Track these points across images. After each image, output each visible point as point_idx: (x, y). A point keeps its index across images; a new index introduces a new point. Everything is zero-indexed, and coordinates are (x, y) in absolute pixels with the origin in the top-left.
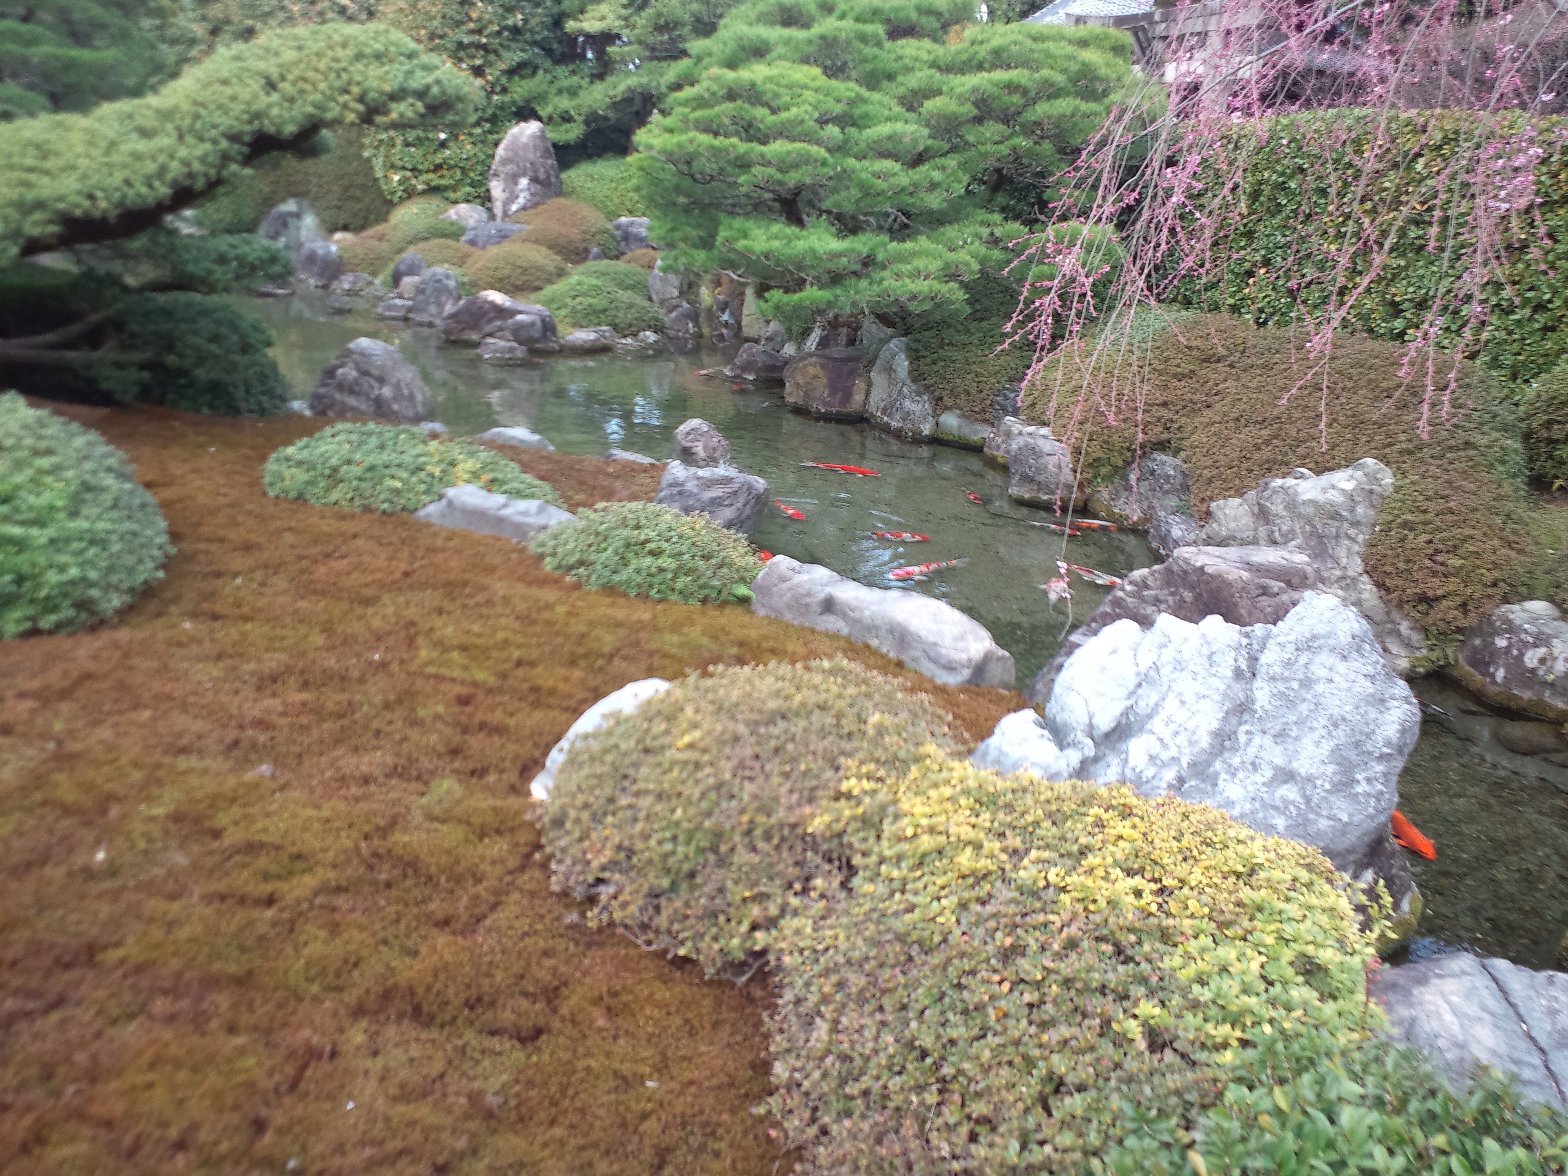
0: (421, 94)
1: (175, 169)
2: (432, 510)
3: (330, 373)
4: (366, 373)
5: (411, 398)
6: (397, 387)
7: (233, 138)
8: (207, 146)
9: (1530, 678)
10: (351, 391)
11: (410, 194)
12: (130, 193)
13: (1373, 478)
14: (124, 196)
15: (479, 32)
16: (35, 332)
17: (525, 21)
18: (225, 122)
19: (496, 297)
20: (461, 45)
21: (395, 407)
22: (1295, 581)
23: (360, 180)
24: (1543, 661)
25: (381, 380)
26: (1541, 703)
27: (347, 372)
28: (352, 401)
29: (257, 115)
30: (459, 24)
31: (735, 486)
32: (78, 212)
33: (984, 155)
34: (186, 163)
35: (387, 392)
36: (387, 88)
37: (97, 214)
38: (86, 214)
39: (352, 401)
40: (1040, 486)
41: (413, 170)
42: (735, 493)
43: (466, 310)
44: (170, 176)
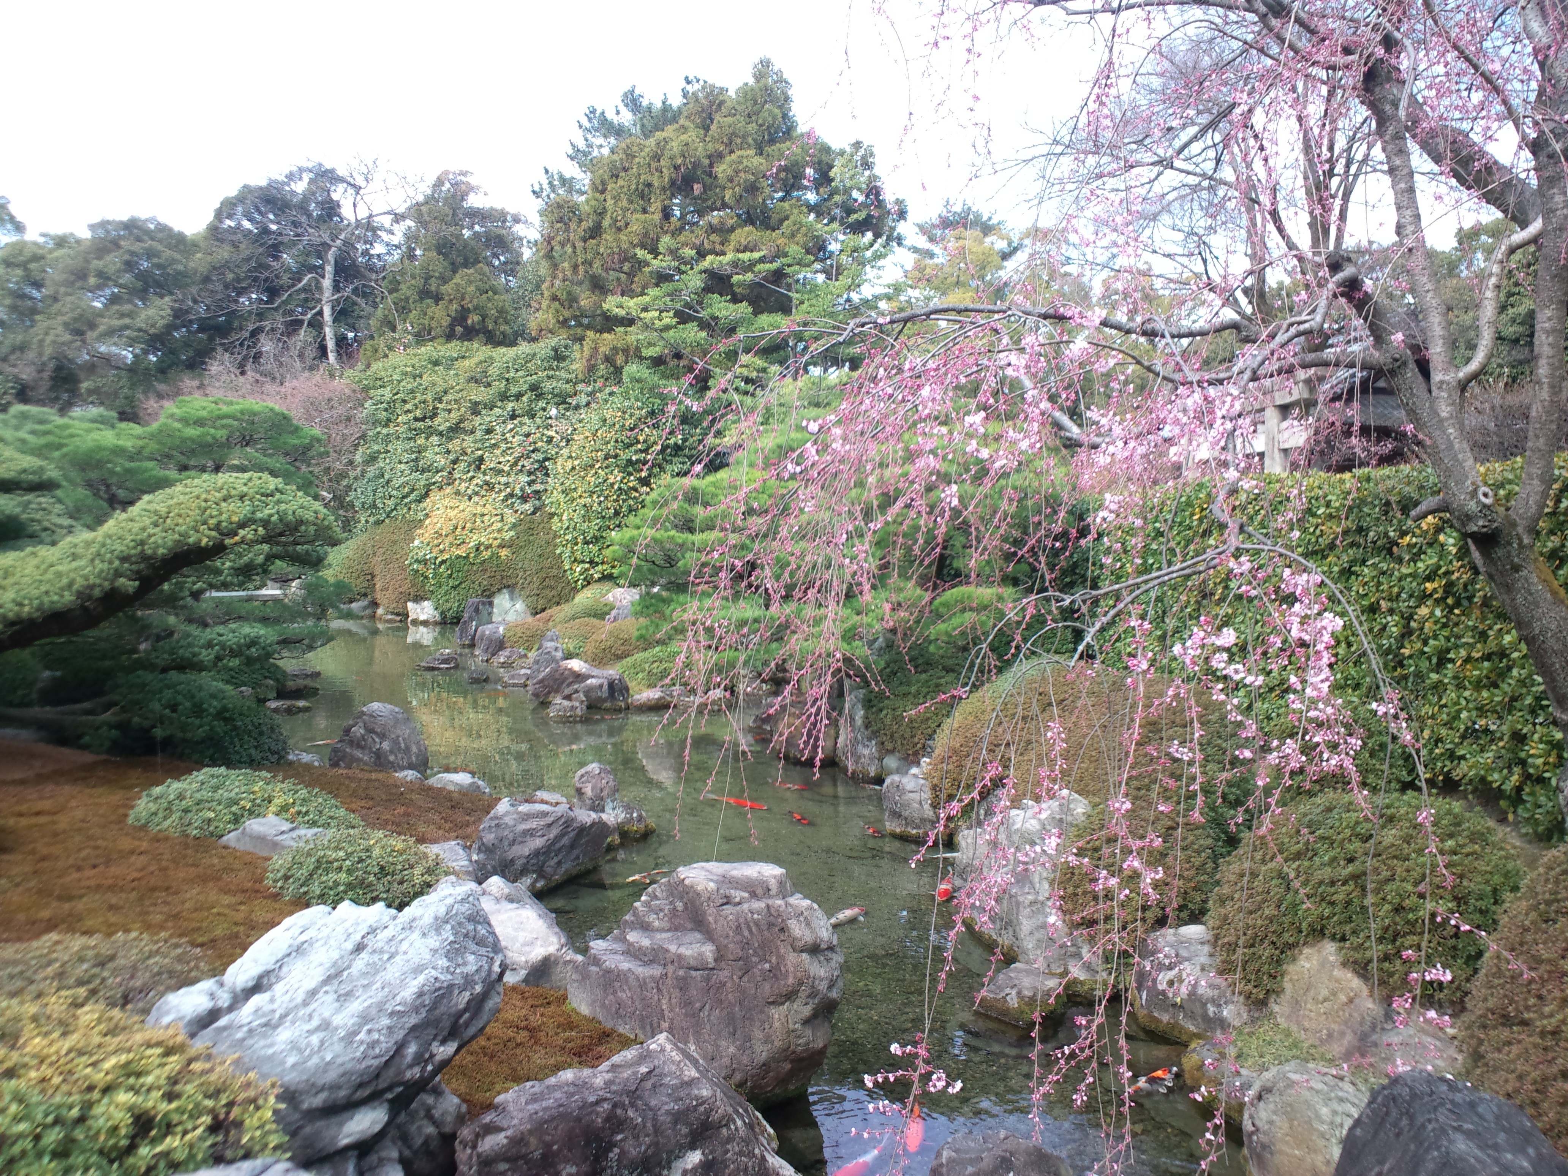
0: (265, 523)
1: (79, 583)
2: (231, 839)
3: (347, 731)
4: (372, 731)
5: (408, 749)
6: (395, 741)
7: (124, 559)
8: (106, 566)
9: (1160, 999)
10: (359, 746)
11: (588, 582)
12: (46, 599)
13: (1066, 808)
14: (42, 603)
15: (646, 451)
16: (76, 701)
17: (685, 440)
18: (119, 547)
19: (576, 665)
20: (630, 462)
21: (392, 758)
22: (759, 891)
23: (554, 572)
24: (1171, 983)
25: (383, 736)
26: (1176, 1026)
27: (358, 731)
28: (358, 754)
29: (142, 543)
30: (628, 446)
31: (549, 820)
32: (11, 615)
33: (59, 575)
34: (86, 578)
35: (386, 745)
36: (235, 519)
37: (24, 615)
38: (18, 615)
39: (358, 754)
40: (908, 822)
41: (591, 562)
42: (549, 826)
43: (551, 675)
44: (75, 587)
